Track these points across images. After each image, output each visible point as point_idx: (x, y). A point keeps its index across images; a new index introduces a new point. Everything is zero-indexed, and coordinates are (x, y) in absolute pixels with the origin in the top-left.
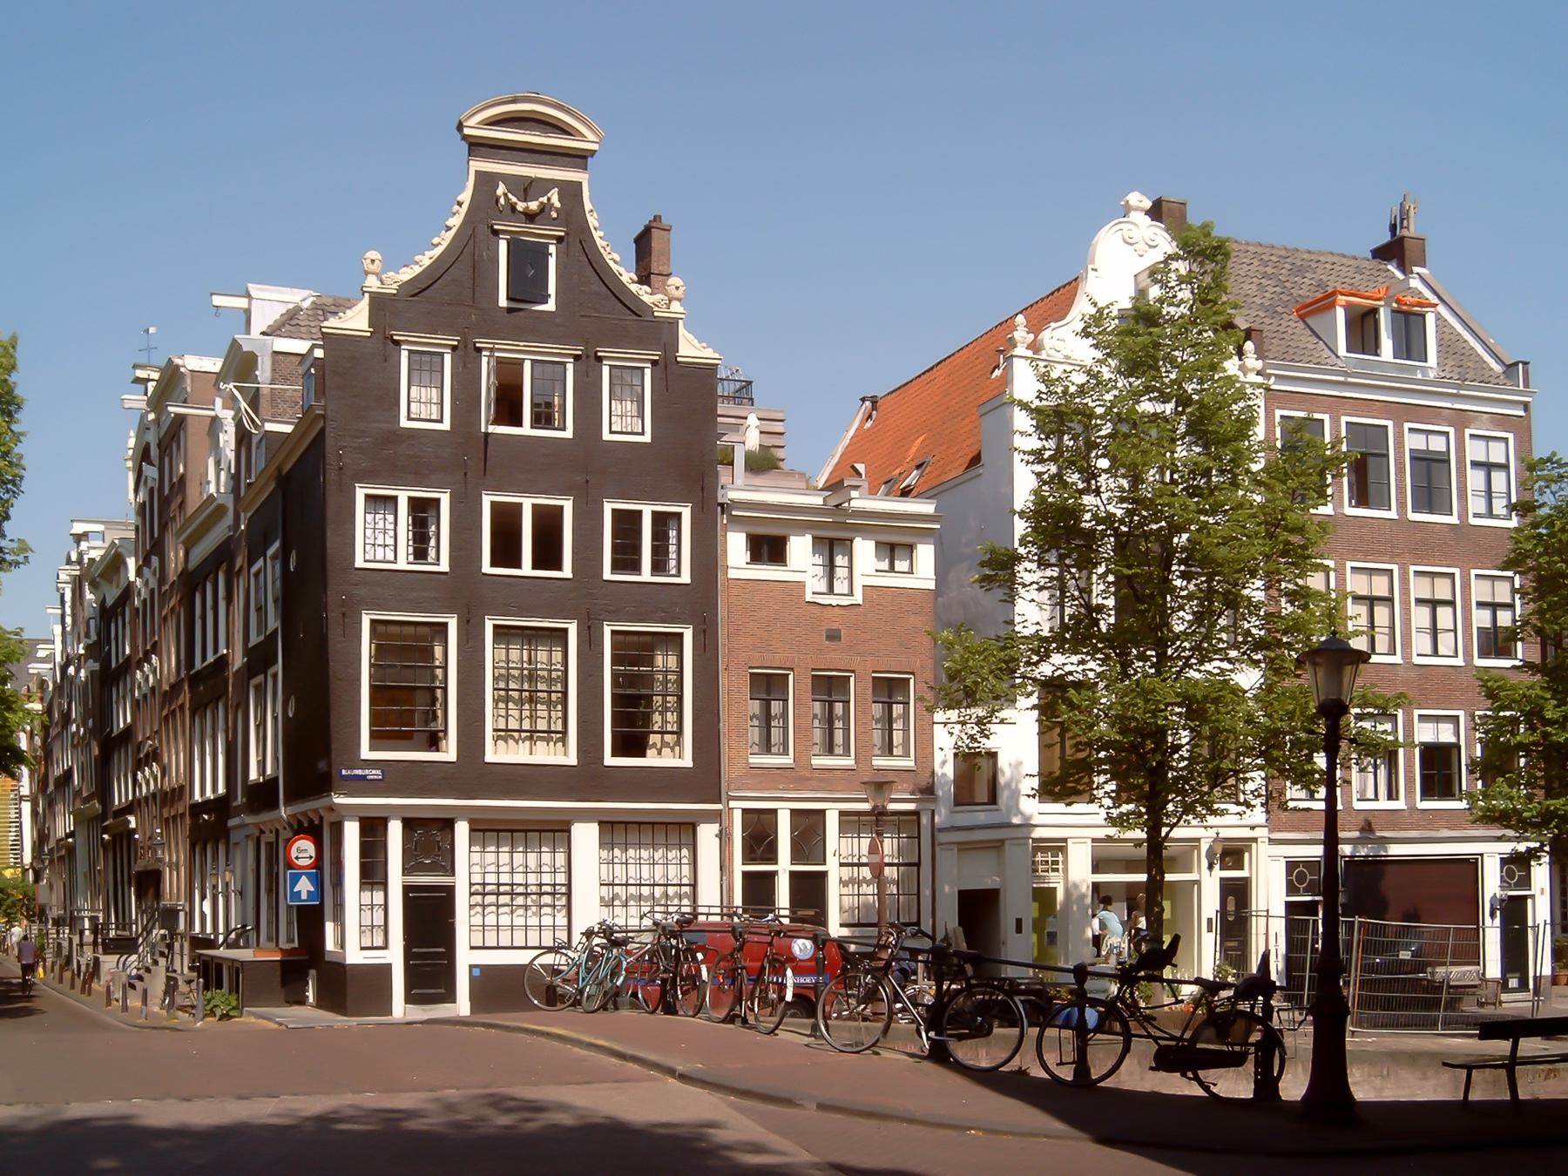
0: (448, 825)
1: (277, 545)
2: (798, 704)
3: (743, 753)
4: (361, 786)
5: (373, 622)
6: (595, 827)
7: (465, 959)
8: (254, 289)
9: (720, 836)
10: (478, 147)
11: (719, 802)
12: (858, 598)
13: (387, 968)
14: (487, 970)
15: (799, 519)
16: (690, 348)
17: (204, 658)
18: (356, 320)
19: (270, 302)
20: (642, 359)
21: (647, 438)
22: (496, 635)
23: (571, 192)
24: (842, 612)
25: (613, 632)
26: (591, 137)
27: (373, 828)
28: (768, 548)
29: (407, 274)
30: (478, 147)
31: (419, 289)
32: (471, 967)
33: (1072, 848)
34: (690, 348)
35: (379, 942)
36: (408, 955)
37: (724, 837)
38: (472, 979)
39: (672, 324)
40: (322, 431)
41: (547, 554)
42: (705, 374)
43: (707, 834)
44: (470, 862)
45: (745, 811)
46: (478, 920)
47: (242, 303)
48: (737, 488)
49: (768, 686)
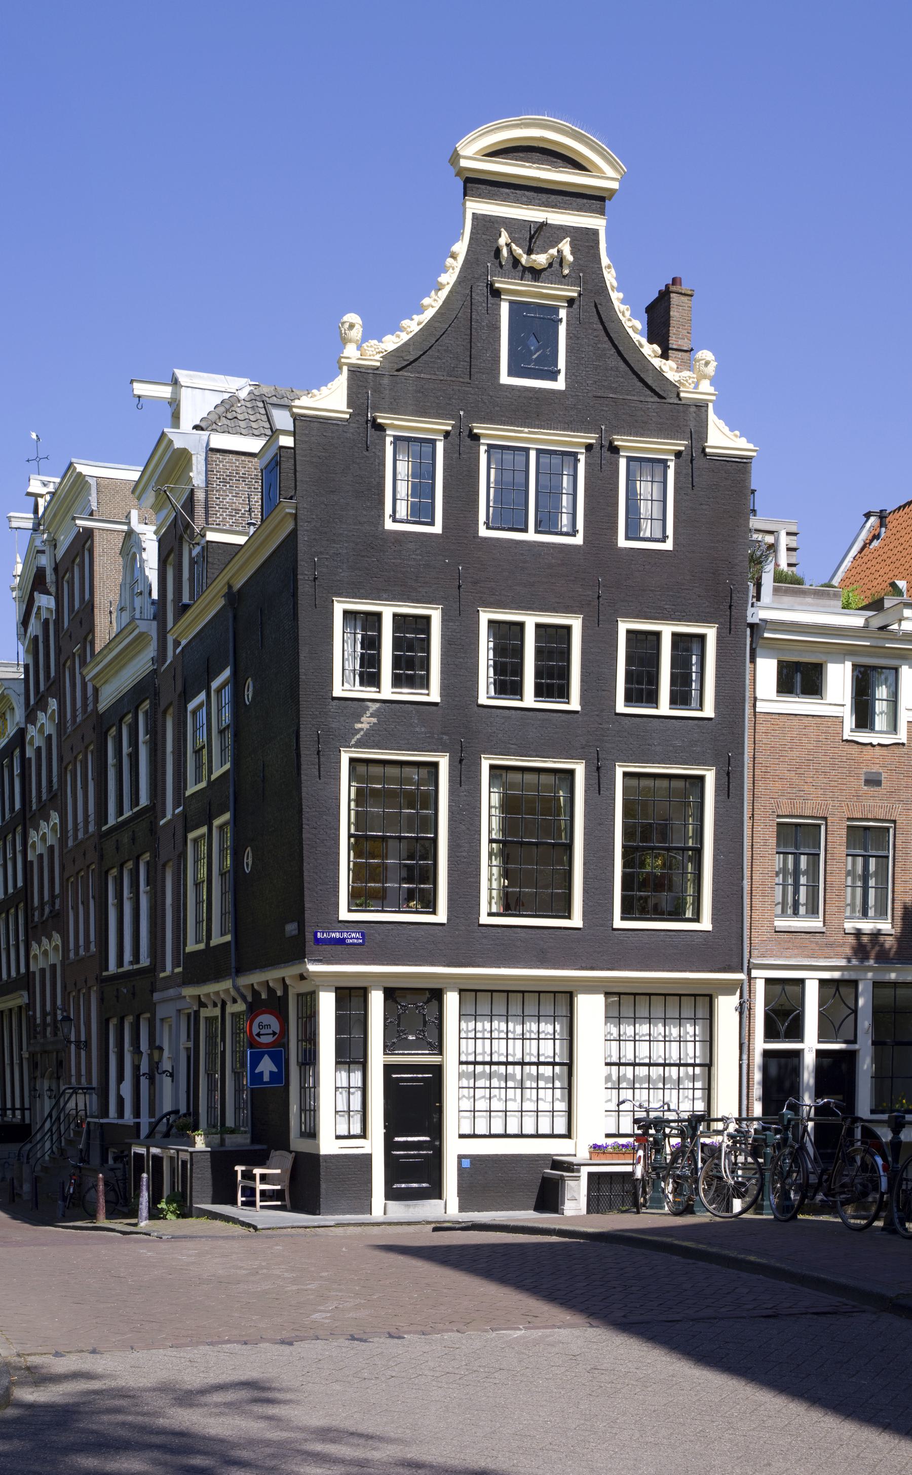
0: (436, 995)
1: (227, 673)
2: (837, 858)
3: (770, 918)
4: (338, 949)
5: (352, 761)
6: (601, 998)
7: (454, 1148)
8: (183, 376)
9: (741, 1009)
10: (476, 184)
11: (741, 970)
12: (902, 736)
13: (367, 1159)
14: (478, 1160)
15: (836, 643)
16: (721, 438)
17: (120, 812)
18: (332, 399)
19: (202, 392)
20: (664, 447)
21: (668, 545)
22: (492, 777)
23: (585, 241)
24: (884, 751)
25: (626, 774)
26: (609, 172)
27: (351, 998)
28: (801, 678)
29: (391, 343)
30: (476, 184)
31: (403, 361)
32: (460, 1157)
33: (808, 983)
34: (721, 438)
35: (356, 1129)
36: (389, 1145)
37: (744, 1010)
38: (461, 1170)
39: (701, 407)
40: (293, 534)
41: (553, 683)
42: (737, 467)
43: (726, 1007)
44: (461, 1037)
45: (769, 981)
46: (467, 1105)
47: (165, 392)
48: (768, 608)
49: (798, 836)
